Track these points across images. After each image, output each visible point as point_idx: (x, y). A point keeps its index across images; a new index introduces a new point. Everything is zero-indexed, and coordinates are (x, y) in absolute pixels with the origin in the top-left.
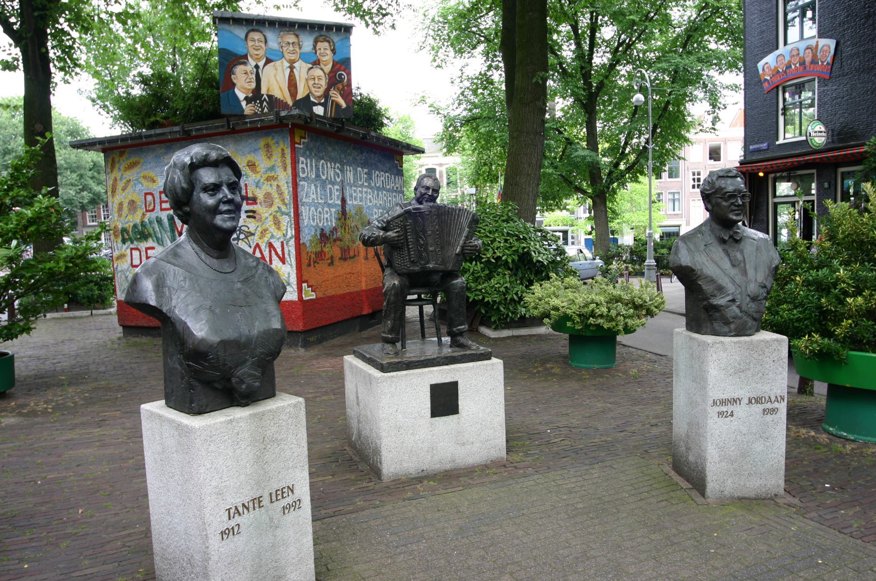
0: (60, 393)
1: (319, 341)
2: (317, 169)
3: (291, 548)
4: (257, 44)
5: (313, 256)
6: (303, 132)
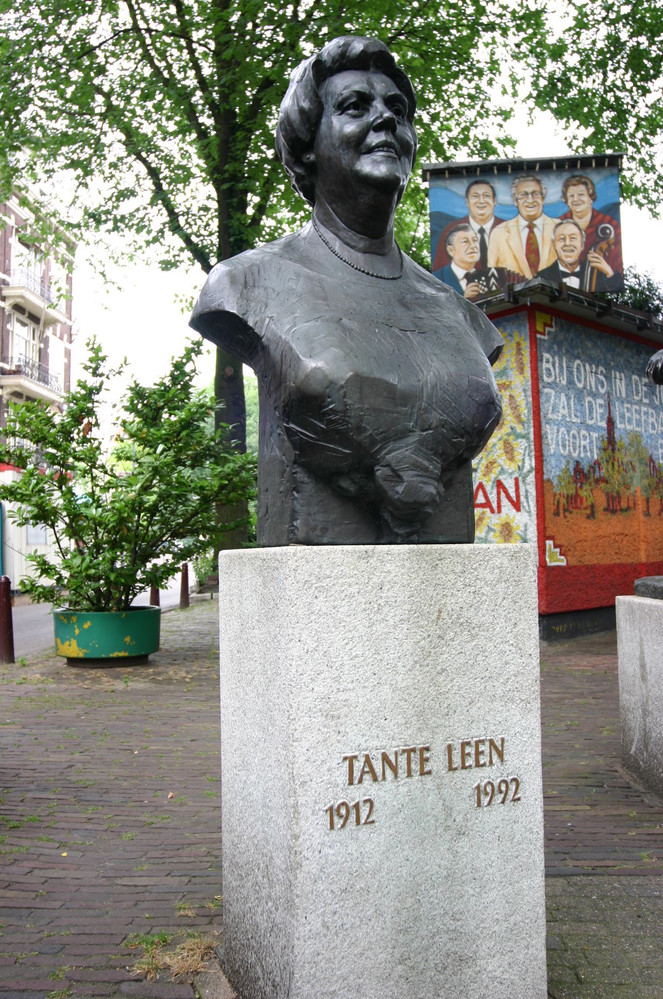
0: (208, 665)
1: (571, 634)
2: (570, 373)
3: (493, 894)
4: (482, 200)
5: (563, 501)
6: (547, 318)
